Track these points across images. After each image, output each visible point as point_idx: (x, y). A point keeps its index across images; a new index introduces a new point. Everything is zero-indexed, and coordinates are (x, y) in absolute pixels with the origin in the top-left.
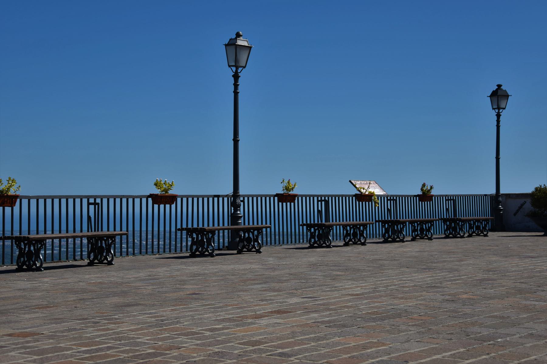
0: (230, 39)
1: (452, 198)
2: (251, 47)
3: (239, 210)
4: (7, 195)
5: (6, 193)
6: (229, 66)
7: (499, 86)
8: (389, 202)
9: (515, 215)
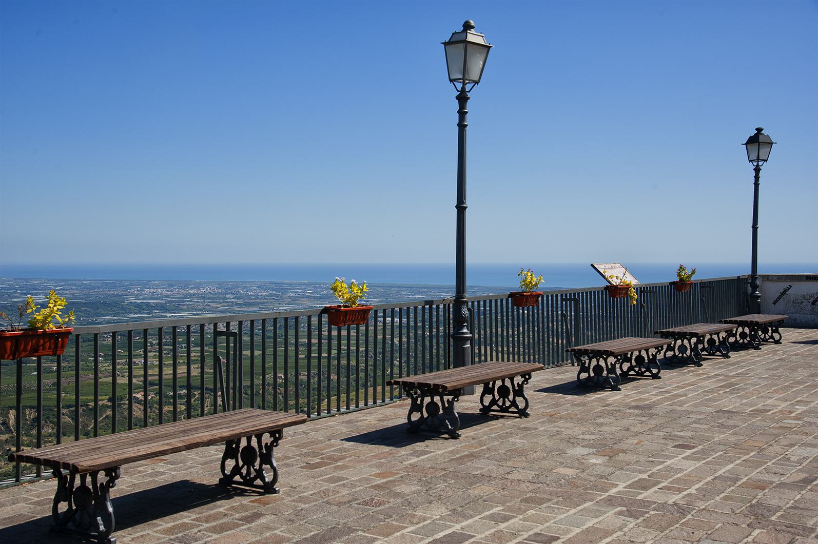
0: (453, 34)
2: (489, 47)
3: (465, 326)
4: (45, 331)
5: (42, 327)
6: (451, 81)
7: (759, 130)
9: (775, 303)
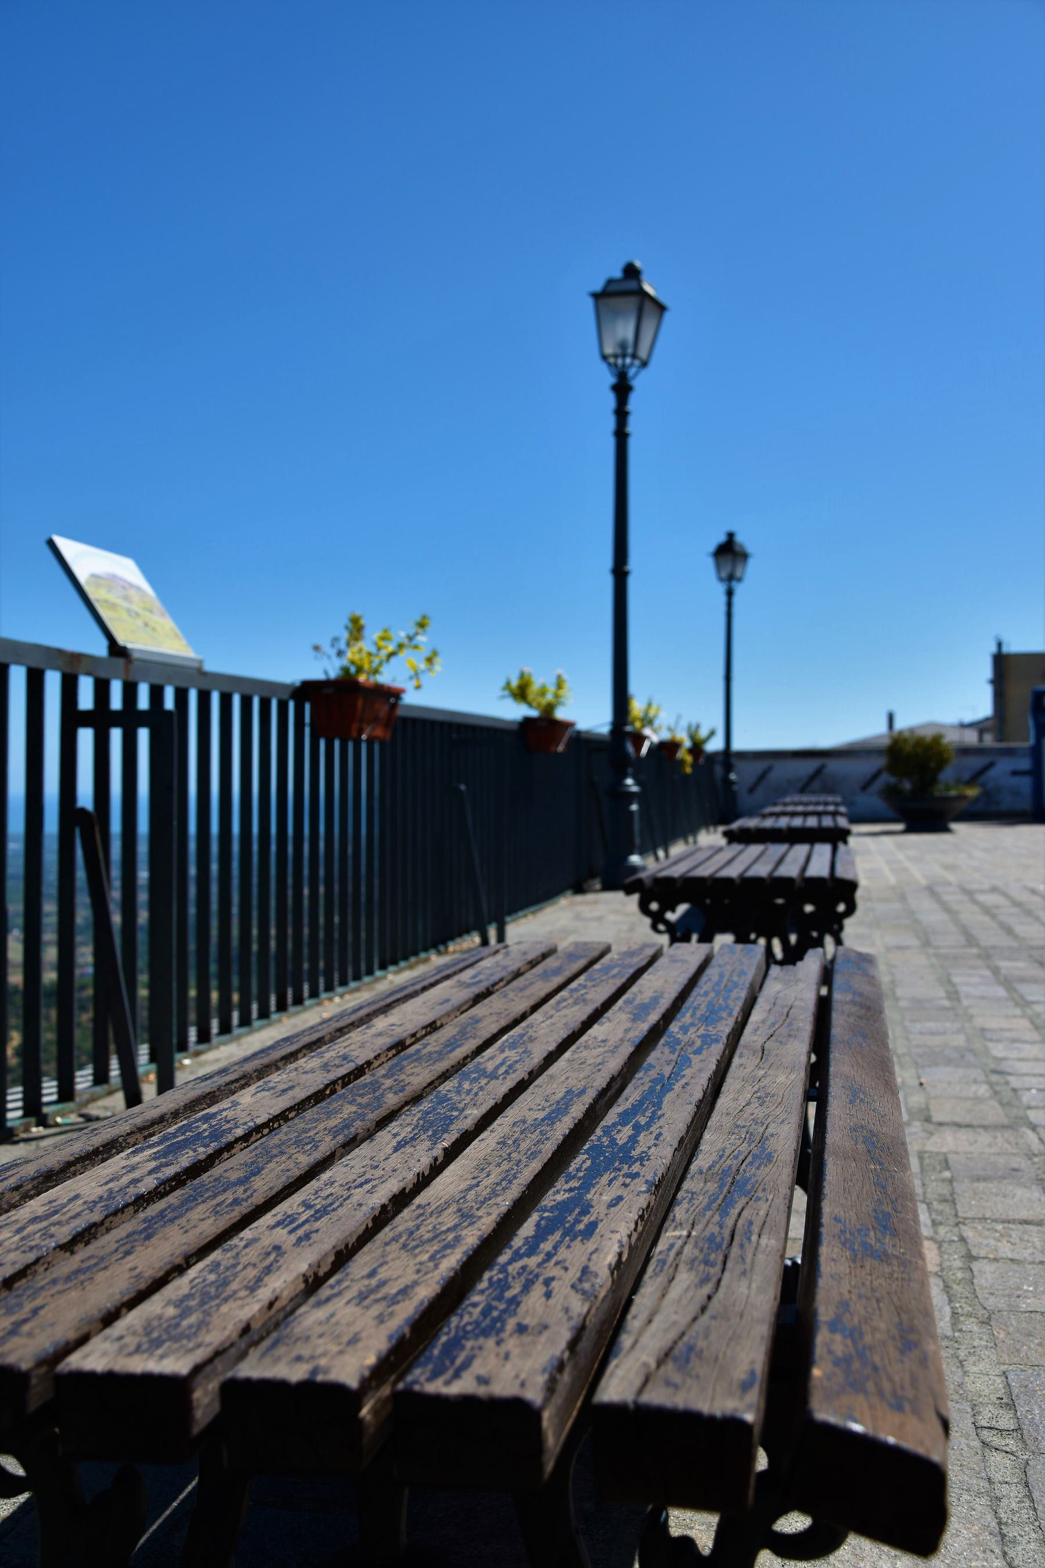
1: (143, 702)
7: (731, 536)
8: (86, 737)
